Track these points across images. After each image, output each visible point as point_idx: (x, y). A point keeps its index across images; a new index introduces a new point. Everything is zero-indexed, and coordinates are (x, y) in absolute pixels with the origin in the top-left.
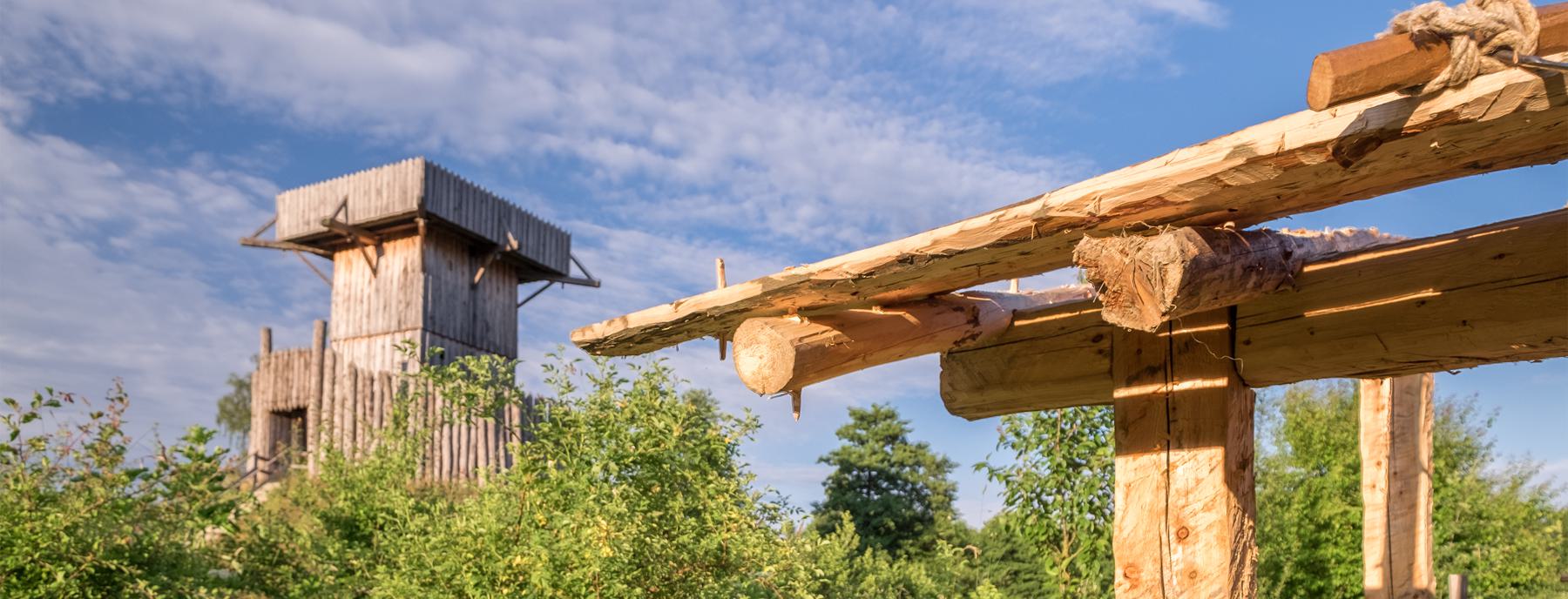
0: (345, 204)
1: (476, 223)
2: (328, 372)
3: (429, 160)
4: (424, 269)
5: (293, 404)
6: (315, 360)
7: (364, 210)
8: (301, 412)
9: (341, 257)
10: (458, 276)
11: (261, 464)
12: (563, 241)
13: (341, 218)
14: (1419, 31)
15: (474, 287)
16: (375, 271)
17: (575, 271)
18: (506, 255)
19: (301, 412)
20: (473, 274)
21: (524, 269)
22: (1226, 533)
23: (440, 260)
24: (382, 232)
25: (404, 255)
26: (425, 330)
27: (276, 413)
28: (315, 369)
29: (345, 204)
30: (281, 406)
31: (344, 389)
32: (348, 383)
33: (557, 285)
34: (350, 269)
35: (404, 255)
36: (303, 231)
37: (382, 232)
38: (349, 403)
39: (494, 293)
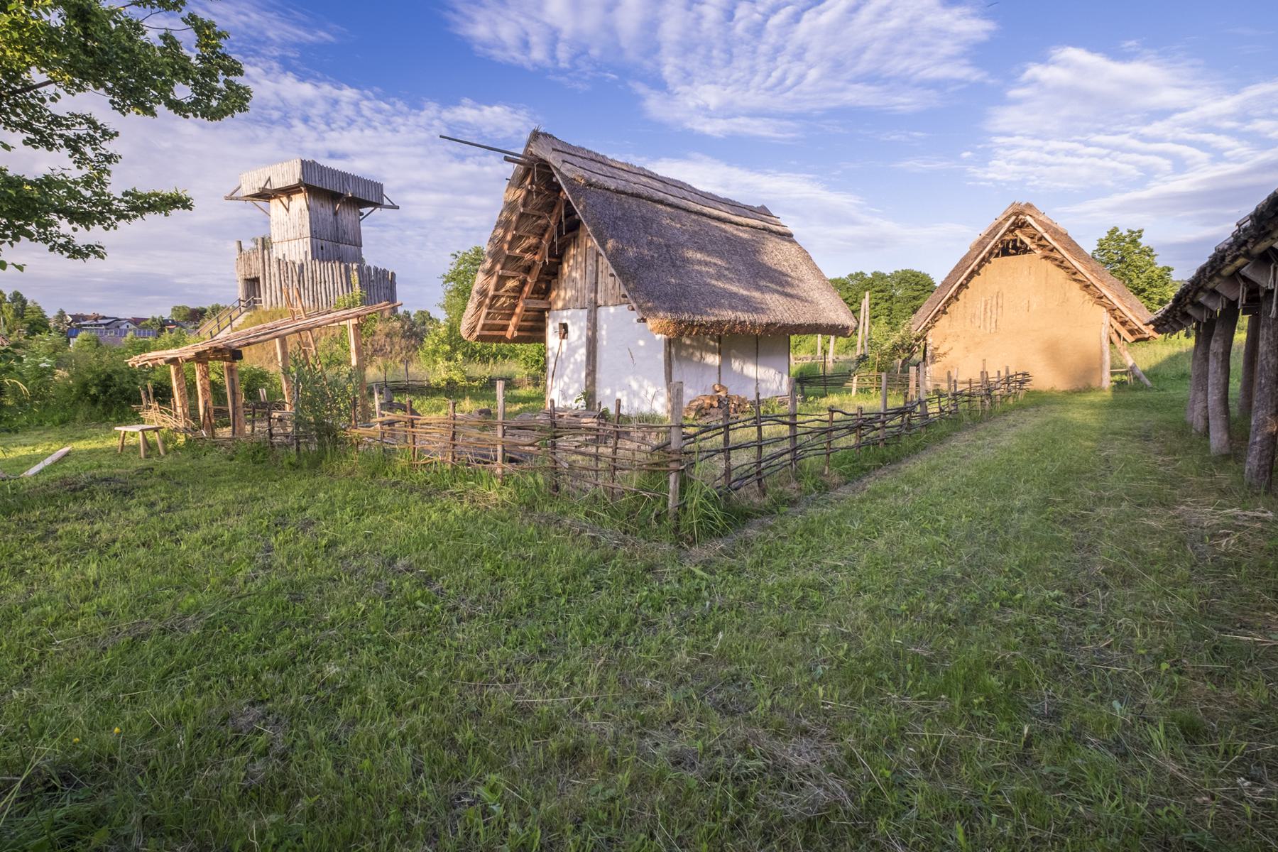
0: (269, 179)
1: (328, 185)
2: (266, 261)
3: (309, 158)
4: (309, 209)
5: (253, 276)
6: (260, 256)
7: (278, 183)
8: (256, 280)
9: (272, 202)
10: (326, 210)
11: (242, 303)
12: (379, 188)
13: (268, 187)
14: (421, 109)
15: (336, 214)
16: (288, 210)
17: (386, 202)
18: (348, 199)
19: (256, 280)
20: (334, 208)
21: (358, 203)
22: (501, 136)
23: (316, 204)
24: (288, 192)
25: (299, 201)
26: (312, 237)
27: (246, 280)
28: (260, 260)
29: (269, 179)
30: (248, 277)
31: (275, 269)
32: (276, 266)
33: (378, 209)
34: (275, 206)
35: (299, 201)
36: (252, 192)
37: (288, 192)
38: (277, 275)
39: (347, 216)
